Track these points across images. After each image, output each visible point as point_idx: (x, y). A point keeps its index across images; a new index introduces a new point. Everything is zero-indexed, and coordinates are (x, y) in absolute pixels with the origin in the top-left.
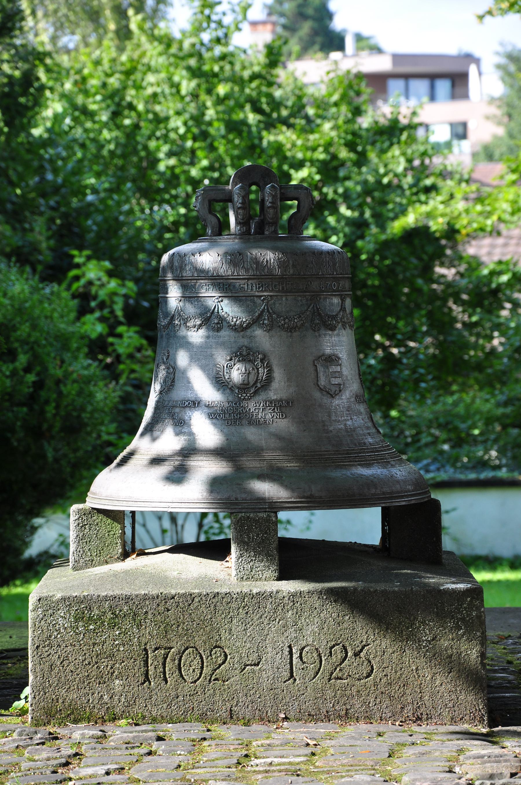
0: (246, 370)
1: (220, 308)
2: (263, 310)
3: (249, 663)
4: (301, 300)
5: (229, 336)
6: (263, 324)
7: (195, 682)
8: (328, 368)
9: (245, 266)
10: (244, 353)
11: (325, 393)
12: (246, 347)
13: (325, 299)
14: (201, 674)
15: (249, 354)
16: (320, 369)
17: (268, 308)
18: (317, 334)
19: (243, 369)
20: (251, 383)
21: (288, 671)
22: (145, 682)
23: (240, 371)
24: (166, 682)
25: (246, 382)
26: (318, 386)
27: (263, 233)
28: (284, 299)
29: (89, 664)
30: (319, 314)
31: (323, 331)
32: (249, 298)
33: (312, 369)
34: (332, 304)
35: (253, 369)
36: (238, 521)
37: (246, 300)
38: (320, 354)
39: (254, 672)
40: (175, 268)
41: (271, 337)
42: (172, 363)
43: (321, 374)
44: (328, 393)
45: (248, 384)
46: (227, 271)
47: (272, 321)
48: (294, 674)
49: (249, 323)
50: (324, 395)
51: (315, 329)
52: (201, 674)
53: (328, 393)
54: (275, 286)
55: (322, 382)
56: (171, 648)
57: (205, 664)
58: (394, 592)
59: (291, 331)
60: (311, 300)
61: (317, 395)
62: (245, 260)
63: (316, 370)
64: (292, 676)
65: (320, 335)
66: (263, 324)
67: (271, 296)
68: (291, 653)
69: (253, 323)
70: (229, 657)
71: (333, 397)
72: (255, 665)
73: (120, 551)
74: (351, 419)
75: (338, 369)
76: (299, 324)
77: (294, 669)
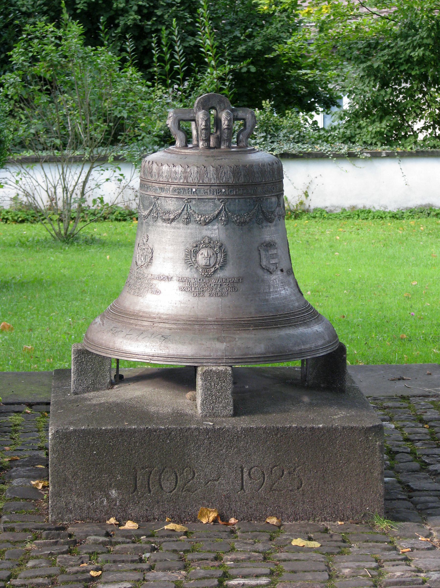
0: (208, 255)
1: (189, 207)
2: (221, 210)
3: (211, 478)
4: (249, 202)
5: (196, 228)
6: (221, 220)
7: (171, 492)
8: (268, 251)
9: (209, 176)
10: (207, 241)
11: (265, 271)
12: (208, 237)
13: (267, 199)
14: (176, 486)
15: (210, 243)
16: (263, 253)
17: (225, 209)
18: (260, 226)
19: (206, 254)
20: (212, 265)
21: (240, 485)
22: (134, 491)
23: (203, 256)
24: (150, 491)
25: (208, 264)
26: (261, 265)
27: (219, 147)
28: (237, 201)
29: (94, 478)
30: (263, 212)
31: (264, 224)
32: (211, 200)
33: (256, 253)
34: (272, 203)
35: (213, 254)
36: (204, 373)
37: (209, 201)
38: (263, 242)
39: (215, 485)
40: (154, 174)
41: (227, 229)
42: (151, 246)
43: (263, 257)
44: (268, 271)
45: (210, 265)
46: (195, 179)
47: (228, 218)
48: (245, 487)
49: (211, 219)
50: (264, 273)
51: (259, 222)
52: (176, 486)
53: (268, 271)
54: (231, 191)
55: (264, 263)
56: (154, 467)
57: (179, 479)
58: (319, 428)
59: (241, 225)
60: (256, 201)
61: (260, 272)
62: (208, 171)
63: (260, 254)
64: (242, 488)
65: (262, 227)
66: (221, 220)
67: (227, 199)
68: (242, 471)
69: (214, 219)
70: (196, 474)
71: (271, 273)
72: (215, 480)
73: (108, 381)
74: (284, 289)
75: (275, 251)
76: (248, 220)
77: (244, 483)
